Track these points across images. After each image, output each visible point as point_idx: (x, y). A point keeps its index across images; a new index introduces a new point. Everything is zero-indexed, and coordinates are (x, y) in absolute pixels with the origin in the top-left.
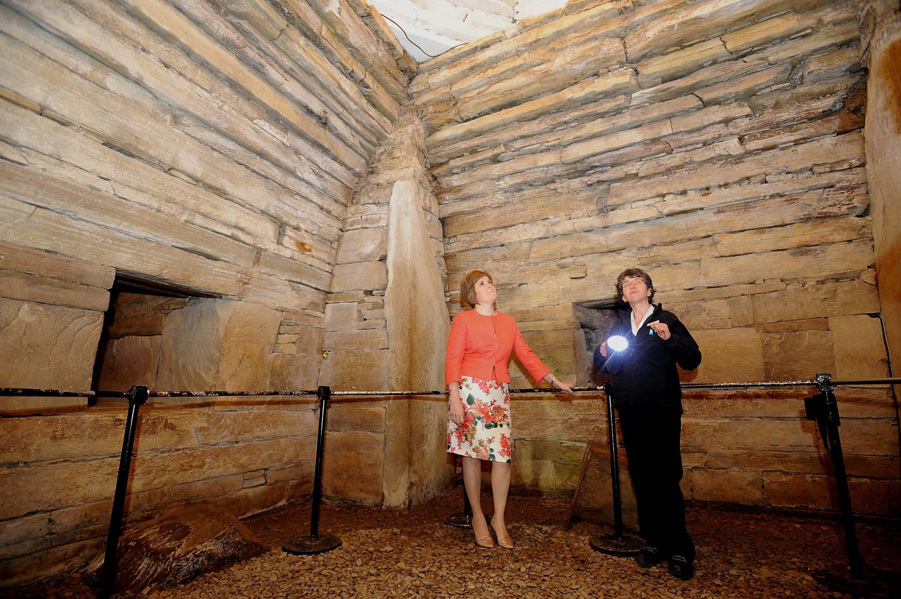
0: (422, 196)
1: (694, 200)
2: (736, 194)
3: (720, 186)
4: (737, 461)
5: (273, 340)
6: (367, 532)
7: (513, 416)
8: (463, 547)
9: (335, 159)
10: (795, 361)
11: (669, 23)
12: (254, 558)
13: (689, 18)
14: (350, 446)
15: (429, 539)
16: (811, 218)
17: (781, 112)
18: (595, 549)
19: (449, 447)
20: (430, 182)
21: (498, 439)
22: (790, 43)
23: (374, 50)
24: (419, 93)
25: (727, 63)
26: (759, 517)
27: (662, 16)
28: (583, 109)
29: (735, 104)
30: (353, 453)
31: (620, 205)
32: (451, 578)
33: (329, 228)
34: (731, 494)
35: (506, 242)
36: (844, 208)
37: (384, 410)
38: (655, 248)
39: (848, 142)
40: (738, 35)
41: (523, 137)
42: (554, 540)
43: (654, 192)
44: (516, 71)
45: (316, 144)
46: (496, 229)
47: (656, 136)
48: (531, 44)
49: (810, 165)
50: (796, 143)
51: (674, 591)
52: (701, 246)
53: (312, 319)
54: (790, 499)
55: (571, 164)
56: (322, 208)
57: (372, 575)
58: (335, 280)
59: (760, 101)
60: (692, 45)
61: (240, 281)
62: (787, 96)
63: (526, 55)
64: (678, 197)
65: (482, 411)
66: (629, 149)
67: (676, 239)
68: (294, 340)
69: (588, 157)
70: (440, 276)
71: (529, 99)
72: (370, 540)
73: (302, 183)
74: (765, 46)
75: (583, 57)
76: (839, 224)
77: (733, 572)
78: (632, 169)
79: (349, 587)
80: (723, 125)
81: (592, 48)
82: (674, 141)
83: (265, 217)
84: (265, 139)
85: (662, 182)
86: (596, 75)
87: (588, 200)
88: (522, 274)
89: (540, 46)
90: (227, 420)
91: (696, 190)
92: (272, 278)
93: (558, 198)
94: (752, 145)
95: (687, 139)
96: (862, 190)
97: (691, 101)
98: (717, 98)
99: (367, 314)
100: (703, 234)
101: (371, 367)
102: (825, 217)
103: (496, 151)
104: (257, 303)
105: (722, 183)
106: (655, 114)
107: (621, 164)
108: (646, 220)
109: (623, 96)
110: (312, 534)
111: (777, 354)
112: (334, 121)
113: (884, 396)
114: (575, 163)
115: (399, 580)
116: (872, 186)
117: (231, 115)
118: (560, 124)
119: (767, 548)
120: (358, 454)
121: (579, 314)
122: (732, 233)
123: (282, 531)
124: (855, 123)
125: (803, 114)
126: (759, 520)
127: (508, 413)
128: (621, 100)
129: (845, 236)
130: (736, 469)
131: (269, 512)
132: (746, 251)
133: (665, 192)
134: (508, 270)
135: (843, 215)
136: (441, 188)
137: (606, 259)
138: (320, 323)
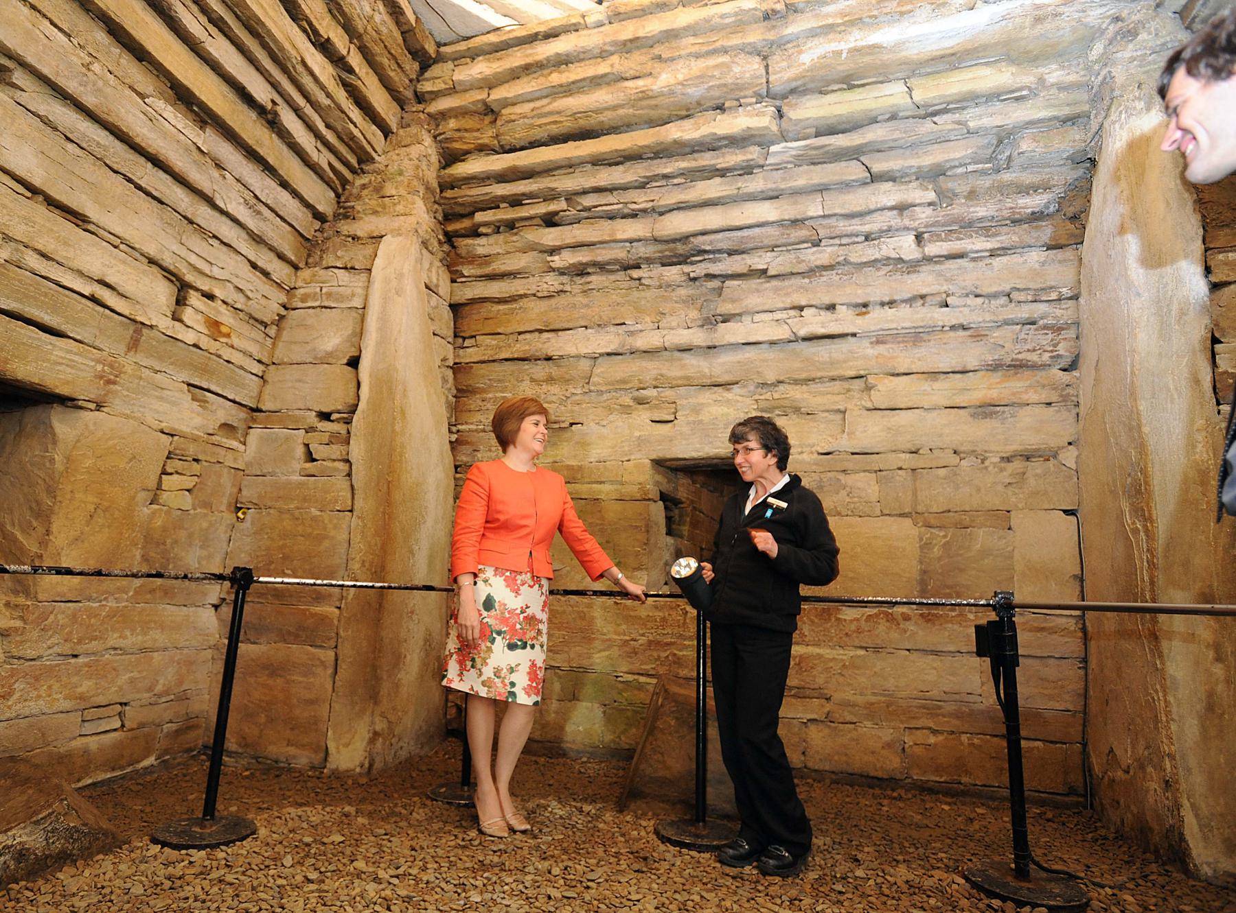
0: (426, 265)
1: (844, 321)
2: (903, 317)
3: (883, 304)
4: (871, 712)
5: (152, 484)
6: (300, 811)
7: (549, 635)
8: (460, 836)
9: (284, 185)
10: (961, 570)
11: (834, 46)
12: (101, 856)
13: (864, 43)
14: (273, 669)
15: (403, 824)
16: (1001, 365)
17: (977, 205)
18: (664, 839)
19: (445, 676)
20: (440, 242)
21: (525, 668)
22: (999, 105)
23: (367, 9)
24: (436, 95)
25: (911, 120)
26: (895, 794)
27: (826, 34)
28: (695, 160)
29: (915, 184)
30: (280, 681)
31: (734, 315)
32: (443, 885)
33: (263, 301)
34: (860, 761)
35: (555, 353)
36: (1047, 355)
37: (337, 611)
38: (781, 387)
39: (1060, 262)
40: (930, 81)
41: (598, 190)
42: (601, 826)
43: (788, 302)
44: (597, 82)
45: (252, 154)
46: (541, 331)
47: (799, 217)
48: (624, 43)
49: (1007, 288)
50: (993, 254)
51: (779, 902)
52: (849, 390)
53: (222, 452)
54: (938, 770)
55: (667, 242)
56: (254, 266)
57: (312, 882)
58: (268, 389)
59: (950, 185)
60: (863, 85)
61: (101, 377)
62: (985, 182)
63: (615, 59)
64: (822, 313)
65: (504, 621)
66: (757, 230)
67: (813, 376)
68: (190, 486)
69: (695, 235)
70: (443, 400)
71: (613, 130)
72: (305, 825)
73: (224, 218)
74: (965, 104)
75: (701, 78)
76: (1038, 378)
77: (860, 873)
78: (758, 261)
79: (272, 903)
80: (895, 212)
81: (717, 66)
82: (824, 227)
83: (155, 269)
84: (165, 135)
85: (801, 287)
86: (721, 108)
87: (690, 301)
88: (576, 408)
89: (638, 48)
90: (60, 617)
91: (848, 305)
92: (158, 376)
93: (643, 294)
94: (932, 249)
95: (844, 226)
96: (1071, 333)
97: (854, 171)
98: (892, 171)
99: (318, 451)
100: (852, 373)
101: (320, 539)
102: (1021, 366)
103: (553, 207)
104: (127, 417)
105: (886, 299)
106: (801, 182)
107: (743, 252)
108: (772, 343)
109: (757, 148)
110: (205, 815)
111: (940, 559)
112: (288, 119)
113: (1072, 624)
114: (674, 241)
115: (358, 890)
116: (1085, 325)
117: (106, 83)
118: (655, 178)
119: (905, 838)
120: (288, 682)
121: (659, 478)
122: (893, 375)
123: (148, 809)
124: (1072, 235)
125: (1006, 213)
126: (895, 798)
127: (544, 628)
128: (753, 153)
129: (1044, 396)
130: (869, 724)
131: (123, 777)
132: (910, 405)
133: (803, 303)
134: (554, 398)
135: (1044, 366)
136: (458, 255)
137: (707, 396)
138: (235, 460)
